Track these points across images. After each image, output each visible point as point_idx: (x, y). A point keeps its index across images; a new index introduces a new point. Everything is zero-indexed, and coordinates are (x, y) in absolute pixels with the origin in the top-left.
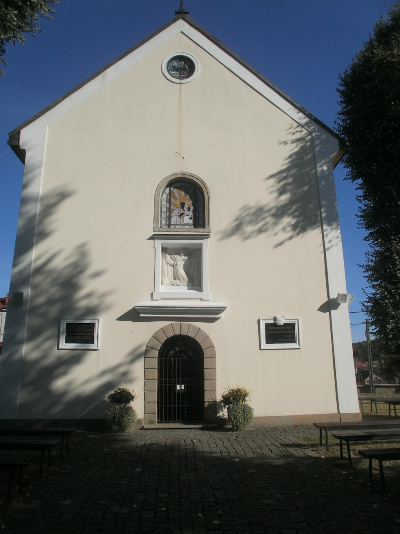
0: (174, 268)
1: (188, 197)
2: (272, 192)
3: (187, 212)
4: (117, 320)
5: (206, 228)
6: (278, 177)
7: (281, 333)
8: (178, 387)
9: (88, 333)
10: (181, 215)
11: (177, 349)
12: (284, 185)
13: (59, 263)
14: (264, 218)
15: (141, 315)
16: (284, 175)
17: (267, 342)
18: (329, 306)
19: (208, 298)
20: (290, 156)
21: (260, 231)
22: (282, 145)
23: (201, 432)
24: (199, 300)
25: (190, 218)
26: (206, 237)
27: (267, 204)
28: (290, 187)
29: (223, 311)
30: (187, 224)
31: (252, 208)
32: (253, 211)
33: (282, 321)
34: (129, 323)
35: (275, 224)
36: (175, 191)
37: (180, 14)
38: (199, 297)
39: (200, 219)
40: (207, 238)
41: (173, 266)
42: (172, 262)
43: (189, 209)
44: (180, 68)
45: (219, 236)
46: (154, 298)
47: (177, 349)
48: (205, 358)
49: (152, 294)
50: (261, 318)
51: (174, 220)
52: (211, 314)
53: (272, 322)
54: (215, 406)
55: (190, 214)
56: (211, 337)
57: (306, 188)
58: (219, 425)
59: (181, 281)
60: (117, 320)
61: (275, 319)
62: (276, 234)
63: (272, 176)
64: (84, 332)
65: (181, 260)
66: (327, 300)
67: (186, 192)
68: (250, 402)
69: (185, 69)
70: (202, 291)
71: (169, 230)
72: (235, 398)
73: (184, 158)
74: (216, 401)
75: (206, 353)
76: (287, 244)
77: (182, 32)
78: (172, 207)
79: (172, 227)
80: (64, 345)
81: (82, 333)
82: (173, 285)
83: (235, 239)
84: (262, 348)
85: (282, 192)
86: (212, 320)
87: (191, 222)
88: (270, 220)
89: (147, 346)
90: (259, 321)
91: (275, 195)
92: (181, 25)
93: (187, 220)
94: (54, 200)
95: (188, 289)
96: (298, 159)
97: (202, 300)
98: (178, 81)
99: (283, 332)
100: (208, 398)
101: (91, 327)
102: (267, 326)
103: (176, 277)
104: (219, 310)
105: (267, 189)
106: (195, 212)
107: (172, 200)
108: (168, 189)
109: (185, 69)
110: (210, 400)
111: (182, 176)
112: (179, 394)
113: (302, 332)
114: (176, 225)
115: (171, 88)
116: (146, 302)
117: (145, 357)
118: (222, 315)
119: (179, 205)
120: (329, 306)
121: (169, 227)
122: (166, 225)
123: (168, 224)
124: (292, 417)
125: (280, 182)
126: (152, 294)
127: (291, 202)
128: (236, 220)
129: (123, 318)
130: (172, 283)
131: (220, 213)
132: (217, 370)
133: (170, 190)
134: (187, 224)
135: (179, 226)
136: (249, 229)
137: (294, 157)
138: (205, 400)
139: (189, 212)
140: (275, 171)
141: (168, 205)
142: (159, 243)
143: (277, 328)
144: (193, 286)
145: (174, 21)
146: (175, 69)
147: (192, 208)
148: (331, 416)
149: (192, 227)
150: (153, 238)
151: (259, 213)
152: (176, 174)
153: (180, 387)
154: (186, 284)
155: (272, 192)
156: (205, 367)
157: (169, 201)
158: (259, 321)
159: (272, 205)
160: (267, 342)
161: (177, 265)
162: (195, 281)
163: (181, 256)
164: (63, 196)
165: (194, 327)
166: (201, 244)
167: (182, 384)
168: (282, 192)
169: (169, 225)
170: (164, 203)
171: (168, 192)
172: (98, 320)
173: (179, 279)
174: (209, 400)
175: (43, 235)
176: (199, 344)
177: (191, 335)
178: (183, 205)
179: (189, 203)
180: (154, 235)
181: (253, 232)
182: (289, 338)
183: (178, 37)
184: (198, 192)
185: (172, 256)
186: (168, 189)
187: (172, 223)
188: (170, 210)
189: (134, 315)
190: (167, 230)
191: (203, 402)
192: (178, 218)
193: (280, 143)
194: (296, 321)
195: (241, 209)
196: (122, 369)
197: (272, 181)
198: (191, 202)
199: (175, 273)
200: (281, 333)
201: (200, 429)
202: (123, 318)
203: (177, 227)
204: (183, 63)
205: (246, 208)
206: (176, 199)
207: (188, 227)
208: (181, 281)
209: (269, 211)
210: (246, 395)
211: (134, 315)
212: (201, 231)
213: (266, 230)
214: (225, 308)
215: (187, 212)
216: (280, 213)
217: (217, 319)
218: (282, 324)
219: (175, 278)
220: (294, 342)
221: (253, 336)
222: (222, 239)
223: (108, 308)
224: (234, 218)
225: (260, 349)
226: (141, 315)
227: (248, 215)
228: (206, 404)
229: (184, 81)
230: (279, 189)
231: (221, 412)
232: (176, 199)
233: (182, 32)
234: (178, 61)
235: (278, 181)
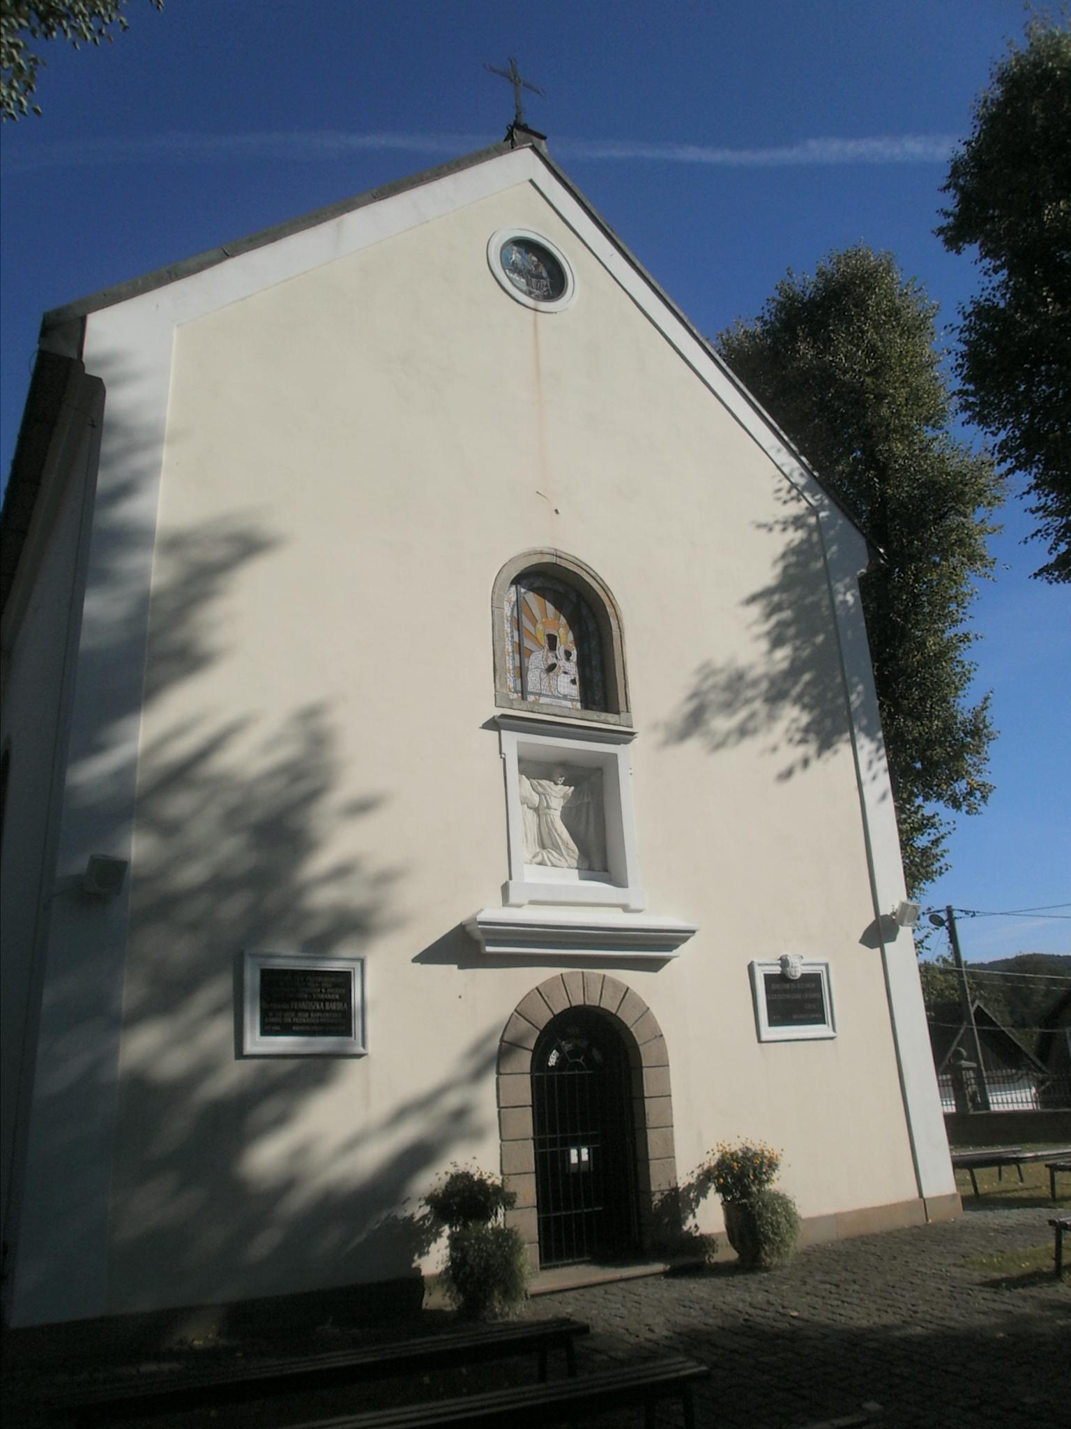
0: (539, 816)
1: (563, 620)
2: (758, 637)
3: (562, 662)
4: (415, 960)
5: (622, 715)
6: (764, 602)
7: (795, 999)
8: (574, 1159)
9: (329, 1001)
10: (552, 668)
11: (567, 1047)
12: (780, 624)
13: (246, 758)
14: (748, 701)
15: (489, 949)
16: (776, 598)
17: (772, 1023)
18: (879, 933)
19: (641, 904)
20: (784, 556)
21: (743, 732)
22: (764, 531)
23: (664, 1282)
24: (620, 910)
25: (573, 682)
26: (625, 737)
27: (751, 667)
28: (792, 631)
29: (685, 940)
30: (565, 697)
31: (721, 671)
32: (722, 679)
33: (798, 969)
34: (449, 972)
35: (772, 718)
36: (532, 599)
37: (517, 133)
38: (622, 901)
39: (600, 684)
40: (627, 742)
41: (537, 810)
42: (536, 798)
43: (568, 654)
44: (529, 271)
45: (660, 735)
46: (512, 900)
47: (567, 1047)
48: (645, 1070)
49: (505, 889)
50: (756, 961)
51: (533, 678)
52: (651, 948)
53: (777, 970)
54: (680, 1203)
55: (572, 667)
56: (655, 1011)
57: (820, 639)
58: (689, 1257)
59: (562, 855)
60: (415, 960)
61: (784, 962)
62: (775, 749)
63: (753, 599)
64: (320, 1000)
65: (558, 794)
66: (874, 918)
67: (559, 607)
68: (779, 1183)
69: (539, 277)
70: (626, 887)
71: (524, 705)
72: (740, 1177)
73: (557, 511)
74: (676, 1189)
75: (647, 1055)
76: (799, 775)
77: (531, 181)
78: (528, 644)
79: (531, 698)
80: (256, 1042)
81: (314, 1004)
82: (541, 863)
83: (694, 745)
84: (764, 1037)
85: (777, 641)
86: (654, 965)
87: (574, 691)
88: (758, 705)
89: (502, 1040)
90: (751, 968)
91: (764, 645)
92: (523, 163)
93: (566, 684)
94: (218, 553)
95: (582, 878)
96: (797, 564)
97: (626, 908)
98: (529, 301)
99: (798, 996)
100: (658, 1184)
101: (343, 981)
102: (769, 979)
103: (547, 841)
104: (670, 940)
105: (749, 626)
106: (582, 664)
107: (526, 623)
108: (513, 589)
109: (539, 277)
110: (665, 1187)
111: (554, 560)
112: (576, 1175)
113: (838, 996)
114: (540, 695)
115: (508, 313)
116: (494, 912)
117: (498, 1073)
118: (683, 949)
119: (544, 641)
120: (879, 933)
121: (524, 698)
122: (516, 692)
123: (519, 688)
124: (837, 1218)
125: (769, 615)
126: (505, 889)
127: (793, 672)
128: (694, 696)
129: (431, 956)
130: (539, 859)
131: (654, 678)
132: (673, 1098)
133: (518, 593)
134: (565, 697)
135: (547, 700)
136: (722, 724)
137: (792, 559)
138: (653, 1189)
139: (567, 664)
140: (757, 587)
141: (516, 634)
142: (512, 740)
143: (787, 986)
144: (590, 869)
145: (511, 143)
146: (513, 268)
147: (574, 653)
148: (907, 1206)
149: (579, 705)
150: (494, 725)
151: (736, 684)
152: (541, 553)
153: (579, 1156)
154: (575, 864)
155: (758, 637)
156: (646, 1094)
157: (518, 624)
158: (751, 968)
159: (759, 670)
160: (772, 1023)
161: (548, 807)
162: (599, 856)
163: (556, 784)
164: (249, 545)
165: (616, 984)
166: (614, 757)
167: (584, 1144)
168: (777, 641)
169: (524, 693)
170: (507, 628)
171: (514, 599)
172: (362, 962)
173: (556, 847)
174: (662, 1188)
175: (189, 661)
176: (627, 1028)
177: (609, 1004)
178: (552, 641)
179: (566, 638)
180: (503, 716)
181: (728, 734)
182: (813, 1011)
183: (511, 191)
184: (585, 611)
185: (535, 782)
186: (513, 589)
187: (530, 688)
188: (521, 651)
189: (463, 947)
190: (577, 714)
191: (649, 1193)
192: (544, 675)
193: (760, 526)
194: (823, 968)
195: (699, 671)
196: (452, 1101)
197: (755, 611)
198: (571, 637)
199: (545, 830)
200: (795, 999)
201: (666, 1274)
202: (431, 956)
203: (543, 700)
204: (534, 259)
205: (707, 670)
206: (534, 621)
207: (569, 704)
208: (562, 855)
209: (755, 683)
210: (773, 1165)
211: (463, 947)
212: (598, 720)
213: (754, 731)
214: (693, 932)
215: (562, 662)
216: (776, 694)
217: (665, 961)
218: (799, 975)
219: (543, 846)
220: (821, 1020)
221: (739, 1006)
222: (666, 743)
223: (398, 923)
224: (688, 692)
225: (760, 1041)
226: (489, 949)
227: (714, 687)
228: (657, 1198)
229: (544, 306)
230: (769, 633)
231: (691, 1217)
232: (534, 621)
233: (531, 181)
234: (523, 251)
235: (768, 609)
